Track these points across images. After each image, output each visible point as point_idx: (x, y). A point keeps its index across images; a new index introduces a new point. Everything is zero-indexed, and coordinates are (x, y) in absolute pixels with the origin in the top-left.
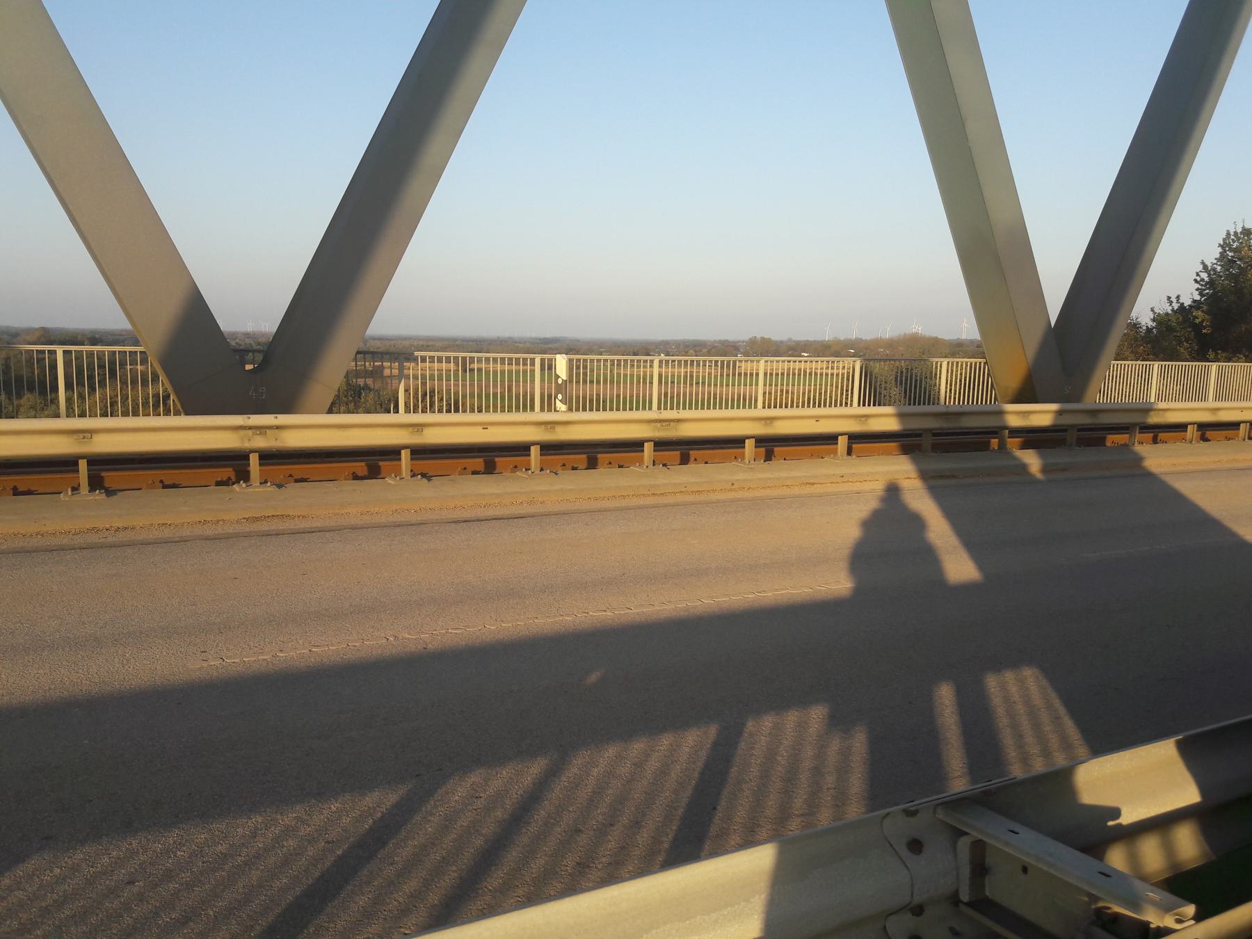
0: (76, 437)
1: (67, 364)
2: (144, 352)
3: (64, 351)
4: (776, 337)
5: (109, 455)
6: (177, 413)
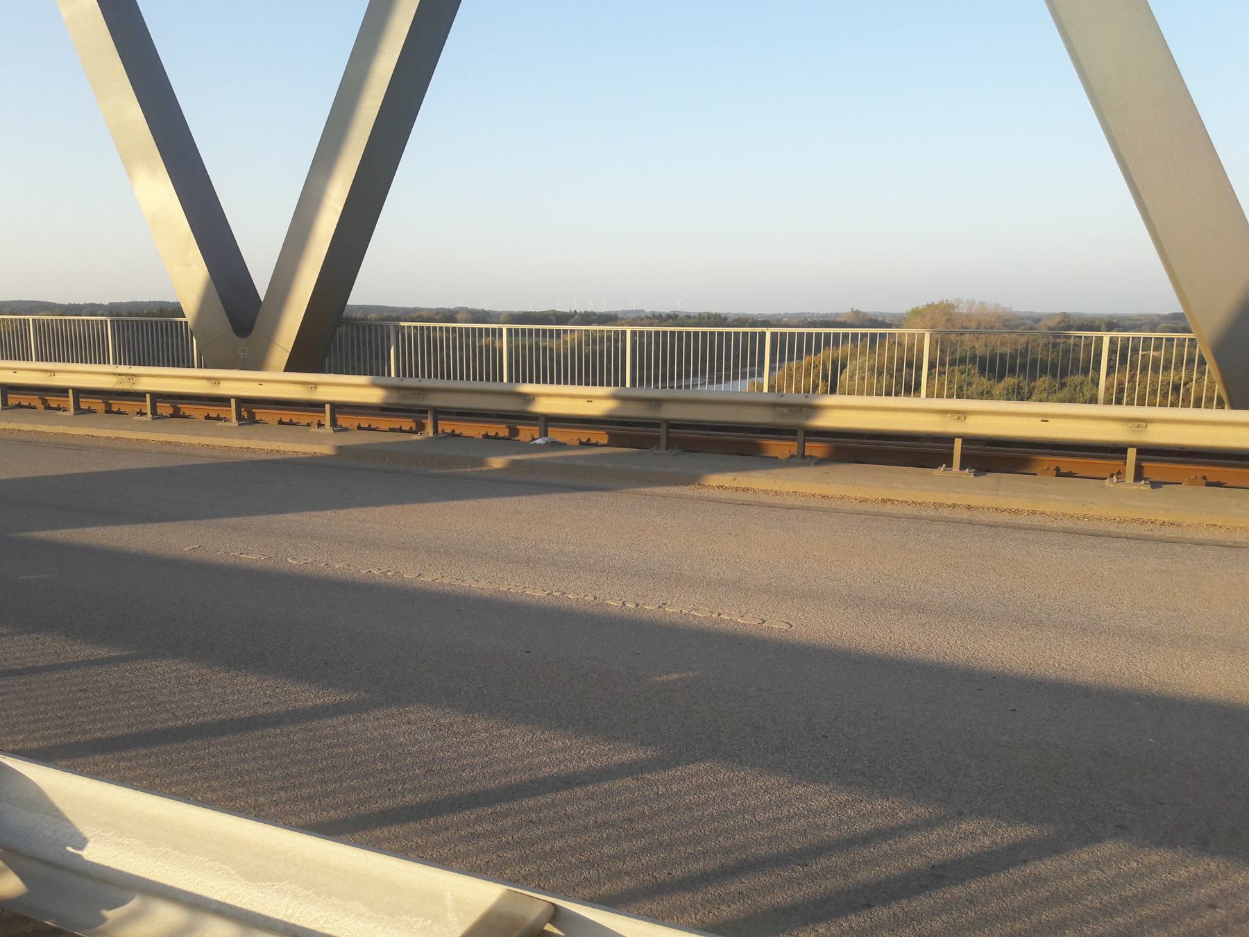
0: (1130, 425)
1: (1112, 351)
2: (1194, 339)
3: (771, 332)
4: (488, 307)
6: (1221, 405)
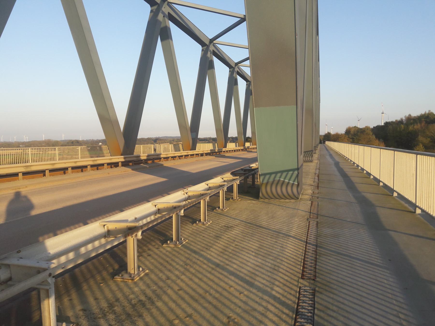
5: (102, 164)
